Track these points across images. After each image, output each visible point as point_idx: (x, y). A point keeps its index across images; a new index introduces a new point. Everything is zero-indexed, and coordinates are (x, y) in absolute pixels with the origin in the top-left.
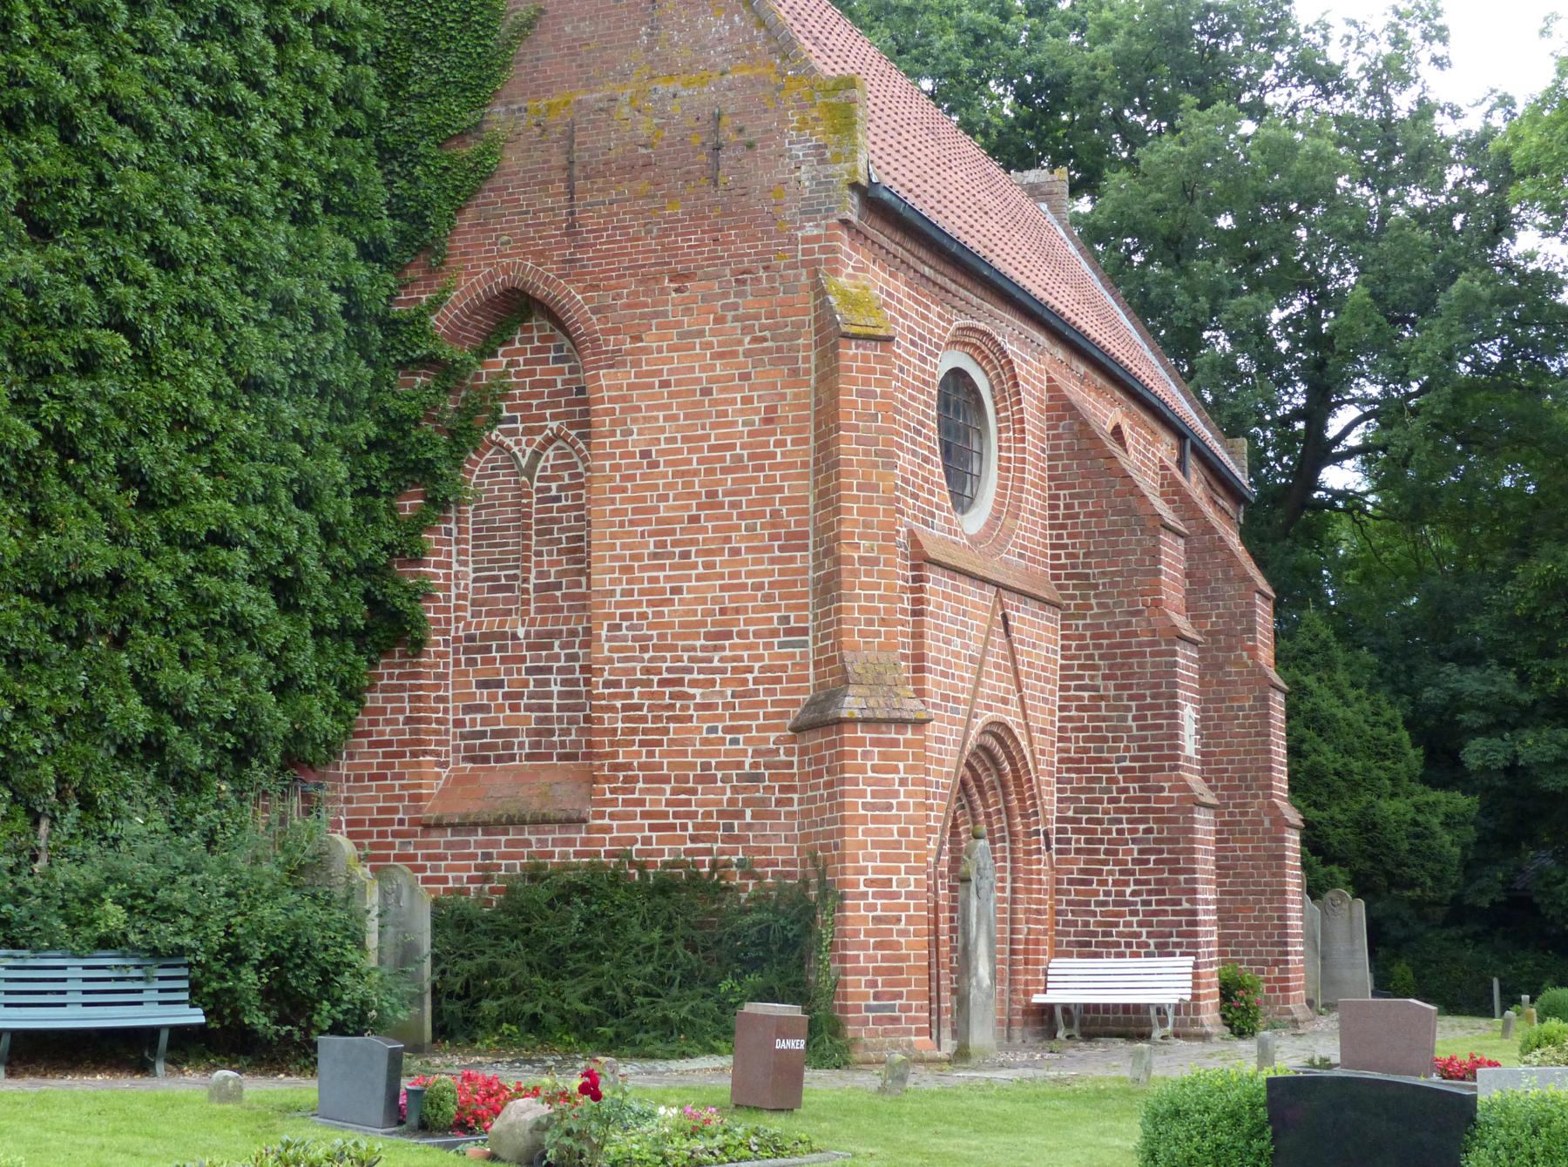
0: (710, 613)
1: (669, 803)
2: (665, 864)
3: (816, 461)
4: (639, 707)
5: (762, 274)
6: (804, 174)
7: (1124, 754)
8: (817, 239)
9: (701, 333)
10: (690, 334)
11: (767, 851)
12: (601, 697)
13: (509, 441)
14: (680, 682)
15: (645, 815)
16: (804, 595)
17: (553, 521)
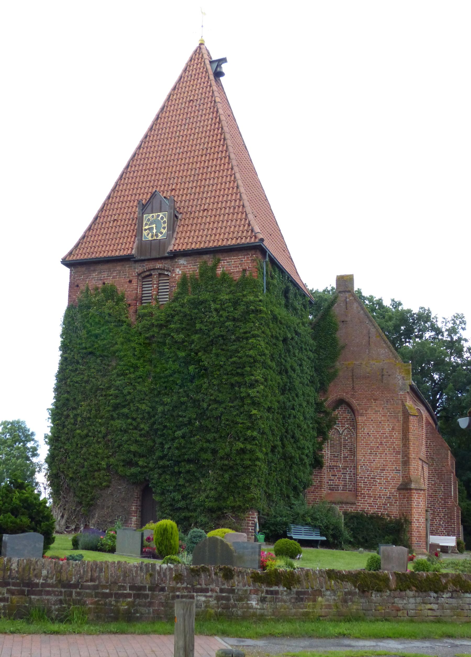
0: (381, 465)
1: (372, 501)
2: (372, 513)
3: (402, 438)
4: (366, 482)
5: (392, 401)
6: (400, 382)
7: (441, 495)
8: (403, 395)
9: (379, 411)
10: (377, 411)
11: (392, 512)
12: (359, 480)
13: (338, 428)
14: (375, 478)
15: (368, 503)
16: (400, 463)
17: (346, 444)
